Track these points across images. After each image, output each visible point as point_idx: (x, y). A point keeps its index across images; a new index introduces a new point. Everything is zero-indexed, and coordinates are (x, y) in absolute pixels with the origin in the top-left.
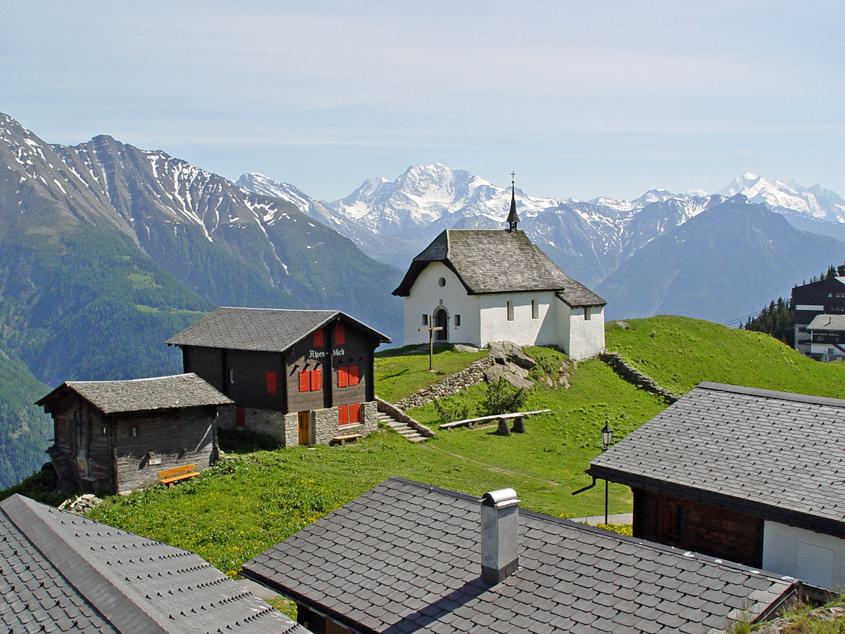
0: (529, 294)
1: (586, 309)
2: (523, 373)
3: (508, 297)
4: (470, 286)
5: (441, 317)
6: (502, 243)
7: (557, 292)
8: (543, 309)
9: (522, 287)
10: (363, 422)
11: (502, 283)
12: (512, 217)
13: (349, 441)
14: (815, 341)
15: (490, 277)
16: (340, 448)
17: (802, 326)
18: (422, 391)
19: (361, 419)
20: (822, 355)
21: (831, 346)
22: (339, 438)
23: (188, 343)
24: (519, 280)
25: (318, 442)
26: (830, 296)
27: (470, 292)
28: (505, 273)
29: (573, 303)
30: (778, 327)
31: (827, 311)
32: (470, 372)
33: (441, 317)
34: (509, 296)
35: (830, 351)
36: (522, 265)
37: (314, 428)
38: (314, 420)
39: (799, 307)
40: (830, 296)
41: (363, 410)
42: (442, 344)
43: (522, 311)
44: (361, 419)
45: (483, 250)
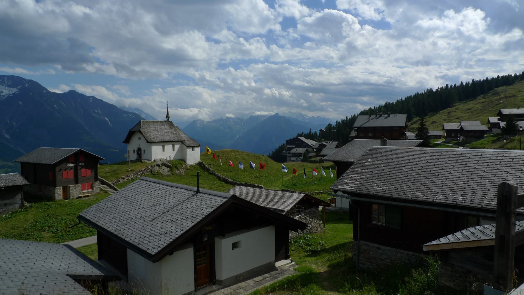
0: (172, 142)
1: (193, 147)
2: (167, 169)
3: (173, 143)
4: (148, 140)
5: (139, 150)
6: (163, 125)
7: (182, 142)
8: (177, 146)
9: (168, 140)
10: (93, 189)
11: (161, 138)
12: (168, 116)
13: (85, 197)
14: (293, 156)
15: (156, 137)
16: (81, 199)
17: (288, 152)
18: (123, 177)
19: (92, 188)
20: (294, 160)
21: (297, 158)
22: (81, 196)
23: (22, 161)
24: (167, 138)
25: (71, 198)
26: (297, 143)
27: (148, 142)
28: (162, 135)
29: (188, 146)
30: (506, 291)
31: (296, 147)
32: (145, 169)
33: (139, 150)
34: (163, 143)
35: (297, 159)
36: (170, 133)
37: (70, 192)
38: (69, 189)
39: (288, 146)
40: (297, 143)
41: (93, 185)
42: (139, 159)
43: (168, 147)
44: (92, 188)
45: (155, 127)
